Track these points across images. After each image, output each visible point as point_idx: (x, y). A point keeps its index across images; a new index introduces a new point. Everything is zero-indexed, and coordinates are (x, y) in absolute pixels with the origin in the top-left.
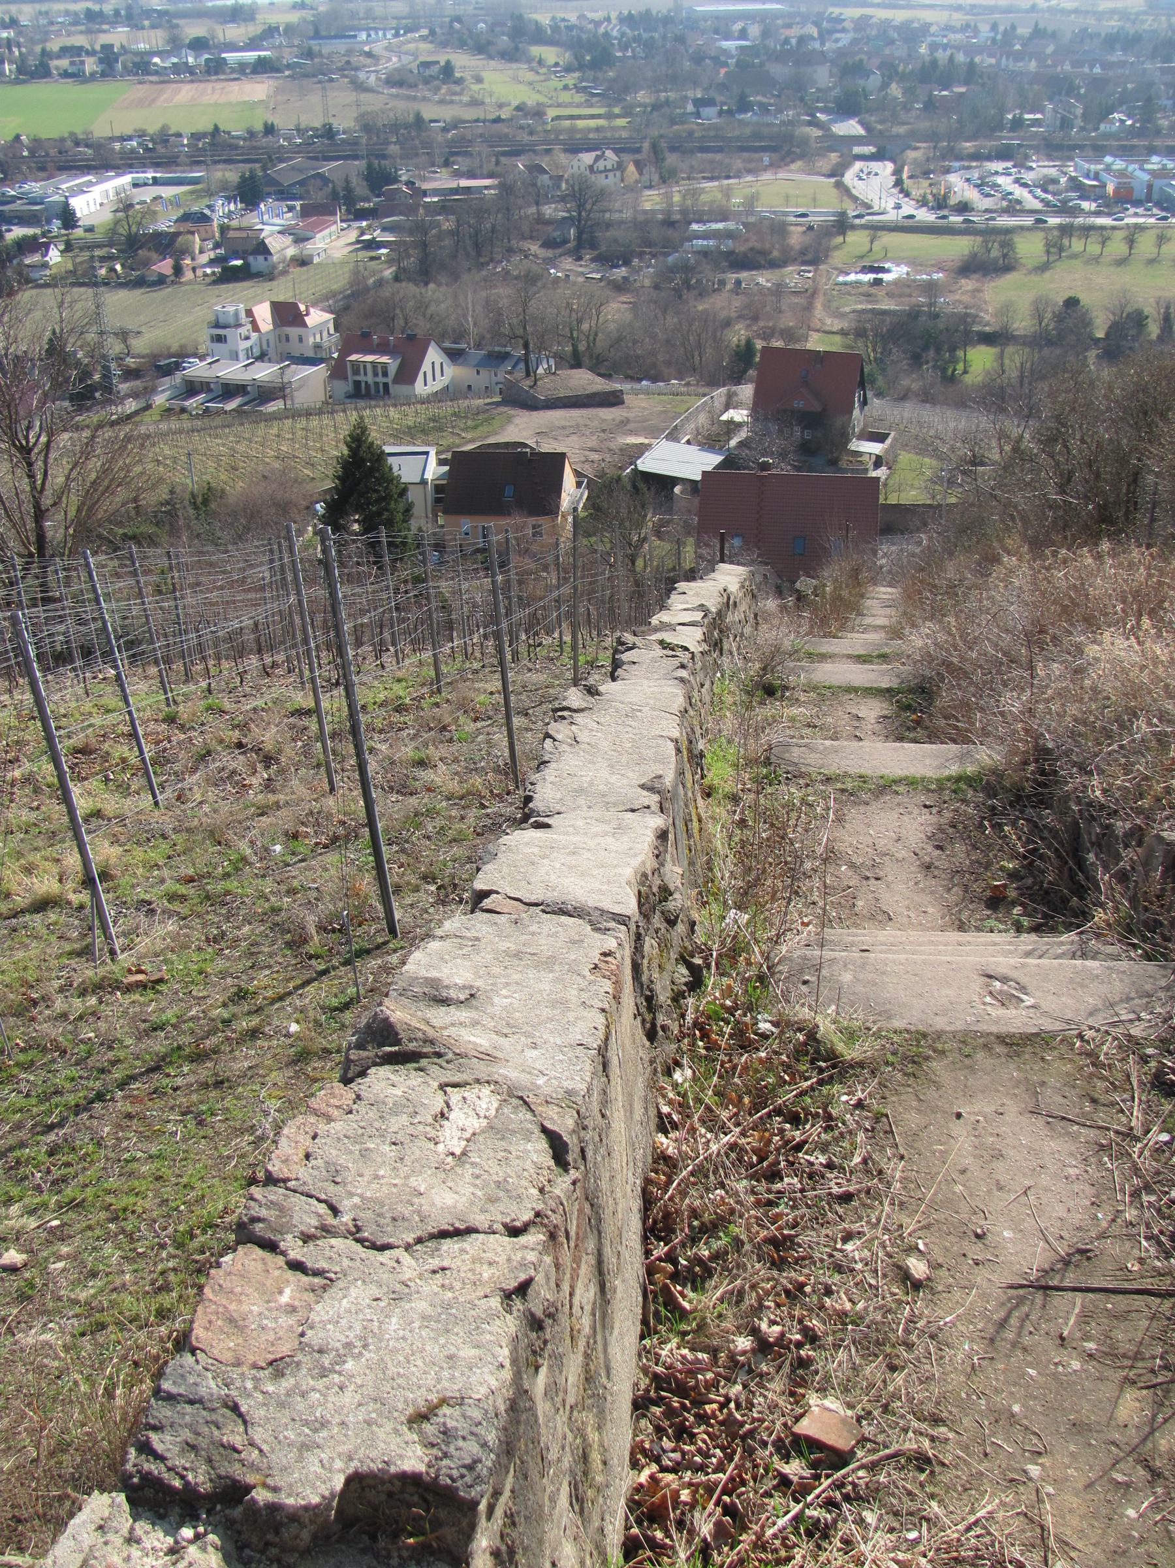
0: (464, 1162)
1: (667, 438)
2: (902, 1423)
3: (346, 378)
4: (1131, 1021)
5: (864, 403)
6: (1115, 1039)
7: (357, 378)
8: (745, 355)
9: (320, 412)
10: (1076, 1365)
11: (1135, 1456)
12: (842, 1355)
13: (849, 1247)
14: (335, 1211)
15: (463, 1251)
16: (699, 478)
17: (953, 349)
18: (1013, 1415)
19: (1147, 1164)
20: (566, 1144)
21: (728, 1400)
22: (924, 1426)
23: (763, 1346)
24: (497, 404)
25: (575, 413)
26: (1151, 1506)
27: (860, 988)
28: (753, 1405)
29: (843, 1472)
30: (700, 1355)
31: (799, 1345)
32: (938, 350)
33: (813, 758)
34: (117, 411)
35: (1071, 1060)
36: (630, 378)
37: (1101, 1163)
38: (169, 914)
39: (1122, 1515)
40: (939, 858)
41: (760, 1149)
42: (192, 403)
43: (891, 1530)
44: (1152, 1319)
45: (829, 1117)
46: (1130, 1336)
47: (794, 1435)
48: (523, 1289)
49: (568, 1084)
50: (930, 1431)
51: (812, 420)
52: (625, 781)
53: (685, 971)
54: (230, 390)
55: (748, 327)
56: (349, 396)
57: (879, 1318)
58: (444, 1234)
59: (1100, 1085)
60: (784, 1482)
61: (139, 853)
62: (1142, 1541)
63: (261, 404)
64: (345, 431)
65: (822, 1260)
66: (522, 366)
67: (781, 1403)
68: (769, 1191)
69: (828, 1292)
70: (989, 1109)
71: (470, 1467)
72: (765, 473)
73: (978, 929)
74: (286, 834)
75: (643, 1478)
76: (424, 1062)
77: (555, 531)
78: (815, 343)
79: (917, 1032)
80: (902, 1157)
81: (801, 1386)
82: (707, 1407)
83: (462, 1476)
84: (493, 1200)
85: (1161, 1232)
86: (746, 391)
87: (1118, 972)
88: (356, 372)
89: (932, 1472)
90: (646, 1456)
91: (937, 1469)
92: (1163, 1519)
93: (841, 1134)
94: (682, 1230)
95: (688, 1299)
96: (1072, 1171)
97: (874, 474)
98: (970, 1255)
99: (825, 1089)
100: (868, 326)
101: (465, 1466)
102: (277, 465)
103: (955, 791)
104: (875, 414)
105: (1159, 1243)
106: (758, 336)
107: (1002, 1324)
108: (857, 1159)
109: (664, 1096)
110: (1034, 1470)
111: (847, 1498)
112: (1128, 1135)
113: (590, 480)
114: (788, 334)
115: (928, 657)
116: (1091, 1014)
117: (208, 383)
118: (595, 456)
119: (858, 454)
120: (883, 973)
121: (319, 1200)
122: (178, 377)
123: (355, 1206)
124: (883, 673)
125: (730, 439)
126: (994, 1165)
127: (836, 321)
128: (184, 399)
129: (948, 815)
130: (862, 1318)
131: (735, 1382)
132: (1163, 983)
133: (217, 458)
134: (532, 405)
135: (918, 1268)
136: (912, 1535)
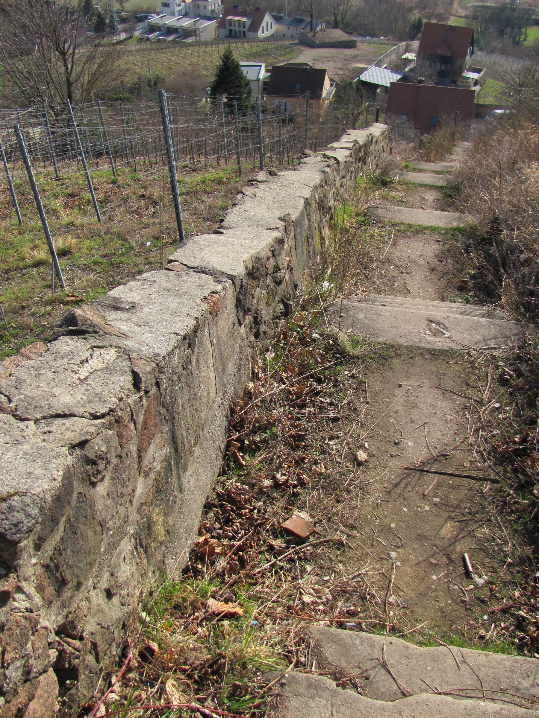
0: (83, 383)
1: (376, 65)
2: (335, 527)
3: (225, 28)
4: (495, 348)
5: (472, 53)
6: (485, 356)
7: (231, 28)
8: (417, 27)
9: (212, 44)
10: (427, 508)
11: (444, 552)
12: (315, 493)
13: (331, 443)
14: (10, 401)
15: (64, 424)
16: (388, 85)
17: (520, 28)
18: (390, 528)
19: (486, 417)
20: (141, 379)
21: (255, 508)
22: (346, 530)
23: (276, 485)
24: (296, 44)
25: (333, 51)
26: (444, 575)
27: (366, 322)
28: (266, 512)
29: (301, 546)
30: (245, 486)
31: (295, 486)
32: (513, 28)
33: (387, 214)
34: (116, 39)
35: (461, 364)
36: (361, 35)
37: (464, 415)
38: (92, 270)
39: (430, 578)
40: (439, 266)
41: (297, 392)
42: (152, 36)
43: (317, 575)
44: (469, 490)
45: (336, 381)
46: (457, 497)
47: (281, 527)
48: (82, 444)
49: (157, 351)
50: (348, 532)
51: (446, 60)
52: (272, 215)
53: (282, 306)
54: (170, 31)
55: (420, 12)
56: (226, 37)
57: (337, 477)
58: (58, 416)
59: (473, 377)
60: (271, 548)
61: (87, 242)
62: (436, 590)
63: (184, 38)
64: (222, 52)
65: (316, 448)
66: (309, 26)
67: (280, 511)
68: (298, 413)
69: (316, 463)
70: (416, 384)
71: (15, 525)
72: (420, 85)
73: (451, 301)
74: (154, 237)
75: (201, 539)
76: (87, 335)
77: (319, 107)
78: (452, 22)
79: (389, 344)
80: (368, 403)
81: (291, 505)
82: (243, 511)
83: (10, 529)
84: (89, 402)
85: (484, 450)
86: (416, 44)
87: (494, 324)
88: (230, 25)
89: (344, 551)
90: (206, 530)
91: (347, 550)
92: (449, 581)
93: (341, 389)
94: (248, 428)
95: (245, 460)
96: (449, 417)
97: (473, 89)
98: (390, 452)
99: (338, 368)
100: (479, 14)
101: (13, 524)
102: (190, 68)
103: (453, 235)
104: (477, 59)
105: (482, 455)
106: (425, 17)
107: (396, 485)
108: (345, 402)
109: (257, 364)
110: (393, 554)
111: (300, 559)
112: (480, 402)
113: (337, 84)
114: (439, 17)
115: (460, 174)
116: (476, 343)
117: (160, 27)
118: (341, 72)
119: (468, 78)
120: (379, 315)
121: (5, 396)
122: (145, 23)
123: (21, 400)
124: (440, 179)
125: (405, 67)
126: (411, 411)
127: (464, 11)
128: (149, 34)
129: (447, 246)
130: (329, 477)
131: (260, 500)
132: (515, 332)
133: (162, 63)
134: (312, 45)
135: (362, 455)
136: (326, 578)
